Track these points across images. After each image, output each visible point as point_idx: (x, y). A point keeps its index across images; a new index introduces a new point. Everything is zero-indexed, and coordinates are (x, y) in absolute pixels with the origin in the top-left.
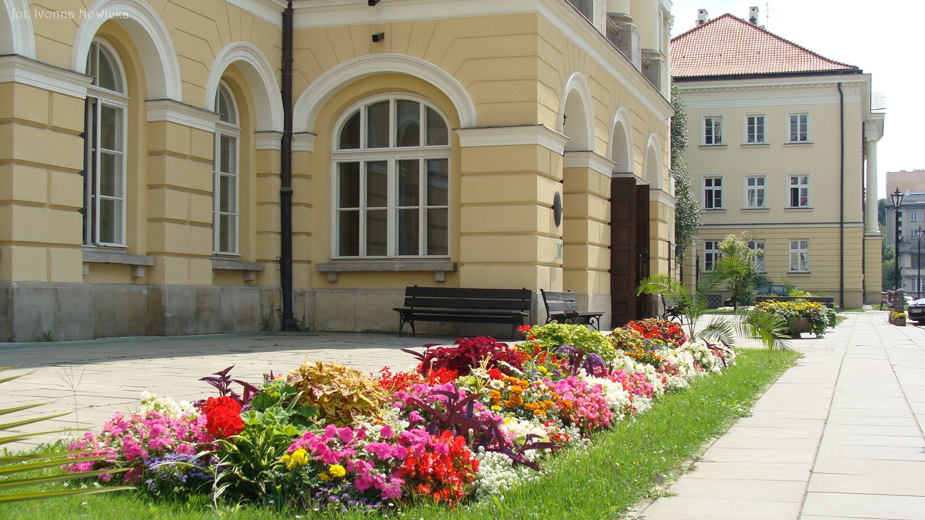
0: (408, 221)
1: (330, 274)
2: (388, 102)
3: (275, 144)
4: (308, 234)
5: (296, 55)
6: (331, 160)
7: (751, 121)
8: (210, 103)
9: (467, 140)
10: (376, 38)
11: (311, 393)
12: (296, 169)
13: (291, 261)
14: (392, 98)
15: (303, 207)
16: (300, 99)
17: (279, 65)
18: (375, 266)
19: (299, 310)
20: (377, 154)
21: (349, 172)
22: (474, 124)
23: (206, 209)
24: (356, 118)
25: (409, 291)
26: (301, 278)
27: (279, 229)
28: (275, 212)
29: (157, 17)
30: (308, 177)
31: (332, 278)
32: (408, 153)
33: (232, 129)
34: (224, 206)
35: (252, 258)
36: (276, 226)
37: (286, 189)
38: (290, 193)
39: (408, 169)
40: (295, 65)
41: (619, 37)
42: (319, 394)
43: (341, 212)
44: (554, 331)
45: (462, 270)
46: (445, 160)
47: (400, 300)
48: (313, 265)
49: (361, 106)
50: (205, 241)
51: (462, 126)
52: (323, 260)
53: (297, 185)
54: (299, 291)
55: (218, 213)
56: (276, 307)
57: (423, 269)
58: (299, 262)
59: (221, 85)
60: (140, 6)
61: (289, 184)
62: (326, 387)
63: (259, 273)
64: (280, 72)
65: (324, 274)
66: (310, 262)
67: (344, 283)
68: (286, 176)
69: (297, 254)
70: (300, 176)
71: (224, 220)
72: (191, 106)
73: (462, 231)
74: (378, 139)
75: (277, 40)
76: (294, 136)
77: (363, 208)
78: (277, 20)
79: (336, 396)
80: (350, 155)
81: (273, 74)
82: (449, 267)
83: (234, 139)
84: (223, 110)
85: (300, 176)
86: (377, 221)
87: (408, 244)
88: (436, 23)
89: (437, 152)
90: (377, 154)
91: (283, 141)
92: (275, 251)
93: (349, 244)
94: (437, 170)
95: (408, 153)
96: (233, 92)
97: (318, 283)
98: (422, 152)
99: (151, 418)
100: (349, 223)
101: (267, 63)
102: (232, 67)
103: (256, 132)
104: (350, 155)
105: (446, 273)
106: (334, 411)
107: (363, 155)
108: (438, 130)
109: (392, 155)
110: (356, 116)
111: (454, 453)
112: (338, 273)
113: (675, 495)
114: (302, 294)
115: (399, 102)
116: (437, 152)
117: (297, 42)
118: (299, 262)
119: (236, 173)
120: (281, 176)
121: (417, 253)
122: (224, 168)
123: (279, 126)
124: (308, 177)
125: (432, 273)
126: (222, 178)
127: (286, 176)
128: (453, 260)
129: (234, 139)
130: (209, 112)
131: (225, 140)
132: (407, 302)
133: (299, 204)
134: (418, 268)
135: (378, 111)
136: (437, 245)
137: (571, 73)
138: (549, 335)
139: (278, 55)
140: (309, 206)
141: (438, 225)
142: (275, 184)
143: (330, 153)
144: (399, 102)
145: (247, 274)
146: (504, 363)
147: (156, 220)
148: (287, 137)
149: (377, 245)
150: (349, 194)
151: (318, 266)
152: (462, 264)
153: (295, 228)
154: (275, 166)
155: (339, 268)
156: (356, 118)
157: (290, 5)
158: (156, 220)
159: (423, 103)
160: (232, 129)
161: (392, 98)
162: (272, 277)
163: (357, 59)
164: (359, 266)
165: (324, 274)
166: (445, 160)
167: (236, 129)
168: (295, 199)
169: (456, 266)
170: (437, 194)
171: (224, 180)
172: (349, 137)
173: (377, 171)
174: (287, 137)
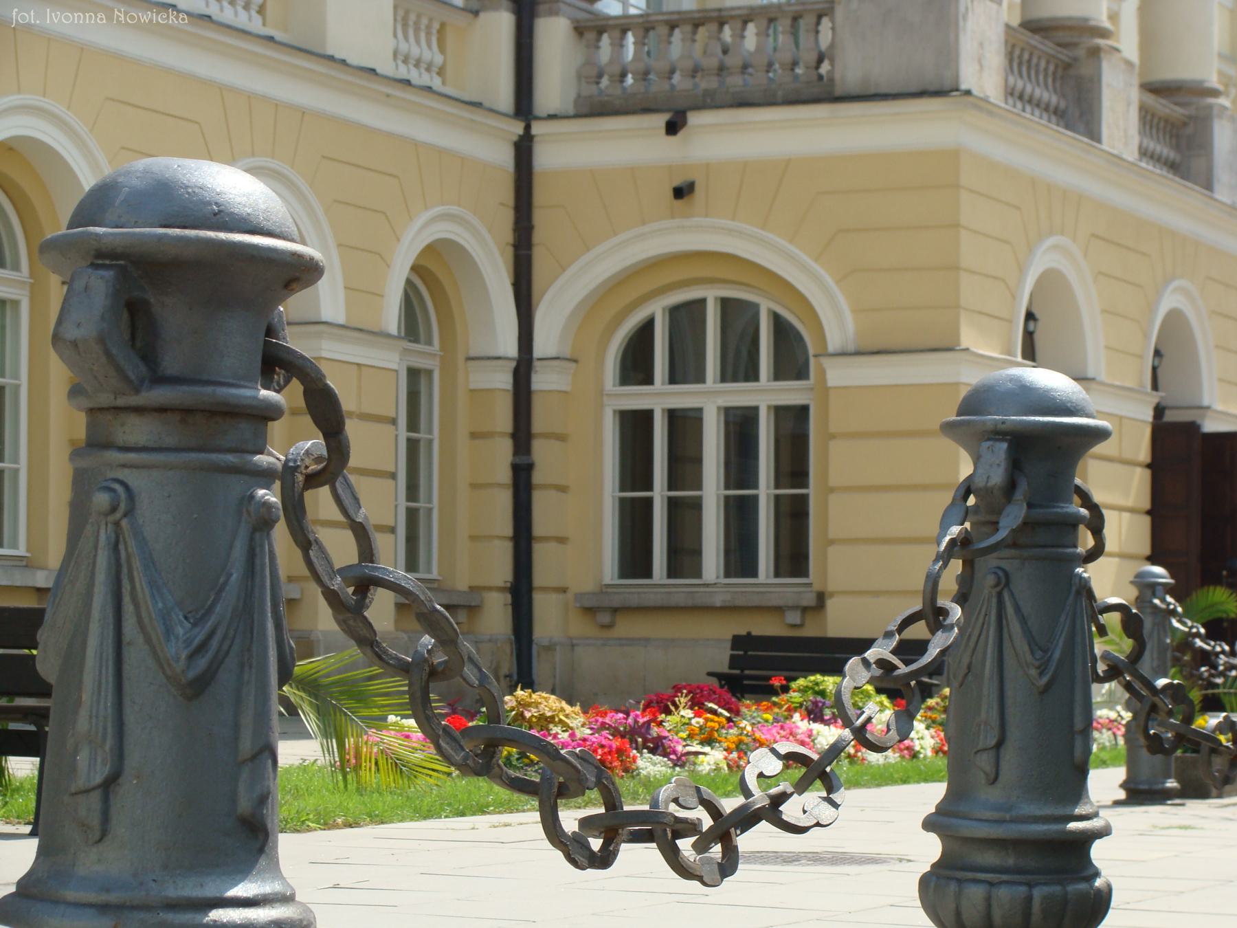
0: (740, 514)
1: (600, 610)
2: (702, 302)
3: (503, 380)
4: (562, 540)
5: (540, 218)
6: (602, 406)
8: (391, 318)
9: (838, 374)
10: (680, 193)
11: (522, 714)
12: (539, 423)
13: (530, 589)
14: (711, 295)
15: (553, 493)
16: (548, 297)
17: (508, 236)
18: (679, 599)
20: (684, 397)
21: (635, 426)
22: (851, 348)
24: (647, 329)
25: (738, 642)
27: (508, 531)
28: (503, 501)
29: (320, 212)
30: (562, 438)
31: (605, 618)
32: (740, 395)
33: (426, 356)
34: (412, 491)
35: (462, 584)
36: (505, 526)
37: (522, 460)
38: (529, 467)
39: (741, 426)
40: (538, 236)
41: (1189, 130)
42: (528, 715)
43: (622, 501)
44: (817, 684)
45: (831, 604)
46: (804, 409)
47: (721, 659)
48: (570, 595)
49: (658, 309)
51: (832, 346)
52: (589, 586)
53: (540, 450)
54: (546, 643)
55: (403, 504)
56: (505, 670)
57: (763, 604)
58: (544, 589)
59: (409, 282)
60: (279, 173)
61: (528, 451)
62: (534, 710)
63: (473, 610)
64: (510, 251)
65: (590, 611)
66: (564, 590)
67: (627, 627)
68: (522, 435)
69: (542, 574)
70: (547, 436)
71: (412, 515)
72: (361, 330)
73: (831, 535)
74: (685, 368)
75: (506, 192)
76: (536, 364)
77: (659, 493)
78: (504, 157)
79: (542, 717)
80: (636, 398)
81: (497, 254)
82: (809, 600)
83: (429, 373)
84: (412, 326)
85: (547, 436)
86: (684, 514)
87: (740, 558)
88: (784, 168)
89: (791, 393)
90: (684, 397)
91: (516, 372)
92: (501, 570)
93: (635, 559)
94: (794, 421)
95: (740, 395)
96: (429, 295)
97: (579, 627)
98: (765, 394)
100: (635, 520)
101: (487, 236)
103: (469, 359)
104: (636, 398)
105: (805, 610)
107: (659, 397)
108: (792, 357)
109: (712, 398)
111: (620, 751)
112: (615, 611)
114: (550, 648)
115: (725, 303)
116: (791, 393)
117: (541, 195)
118: (544, 589)
119: (434, 433)
120: (515, 436)
121: (754, 574)
122: (413, 425)
123: (509, 346)
124: (562, 438)
125: (779, 610)
126: (409, 440)
127: (522, 435)
128: (817, 587)
129: (429, 373)
130: (389, 336)
131: (414, 374)
132: (734, 661)
133: (545, 487)
134: (756, 601)
135: (686, 318)
136: (794, 559)
137: (1051, 233)
138: (812, 688)
139: (506, 218)
140: (562, 489)
142: (503, 450)
143: (601, 392)
144: (725, 303)
146: (711, 705)
149: (684, 557)
150: (635, 470)
151: (579, 596)
152: (832, 595)
153: (538, 529)
154: (503, 420)
155: (616, 601)
156: (647, 329)
157: (528, 128)
159: (766, 308)
160: (426, 356)
161: (711, 295)
163: (646, 229)
164: (652, 598)
165: (590, 611)
166: (804, 409)
167: (433, 355)
168: (538, 477)
169: (821, 598)
170: (794, 466)
171: (413, 445)
172: (636, 364)
173: (684, 425)
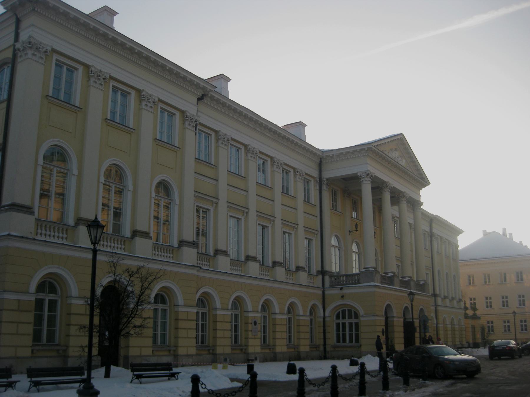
3: (322, 320)
7: (469, 277)
9: (362, 319)
19: (328, 356)
20: (344, 321)
21: (338, 325)
23: (308, 336)
26: (328, 349)
28: (322, 335)
36: (322, 337)
39: (351, 324)
49: (340, 310)
50: (308, 342)
53: (326, 328)
68: (324, 326)
69: (327, 343)
74: (344, 318)
87: (351, 341)
89: (356, 321)
90: (344, 321)
92: (322, 343)
93: (338, 341)
94: (357, 324)
98: (353, 321)
99: (406, 392)
102: (313, 305)
104: (338, 321)
106: (126, 313)
107: (341, 321)
109: (347, 321)
110: (339, 312)
113: (19, 381)
116: (356, 321)
123: (322, 315)
127: (324, 326)
135: (343, 312)
141: (357, 336)
145: (317, 347)
147: (299, 339)
148: (324, 318)
149: (344, 341)
154: (322, 324)
158: (299, 339)
162: (322, 348)
169: (361, 345)
172: (338, 317)
173: (344, 324)
174: (324, 318)
